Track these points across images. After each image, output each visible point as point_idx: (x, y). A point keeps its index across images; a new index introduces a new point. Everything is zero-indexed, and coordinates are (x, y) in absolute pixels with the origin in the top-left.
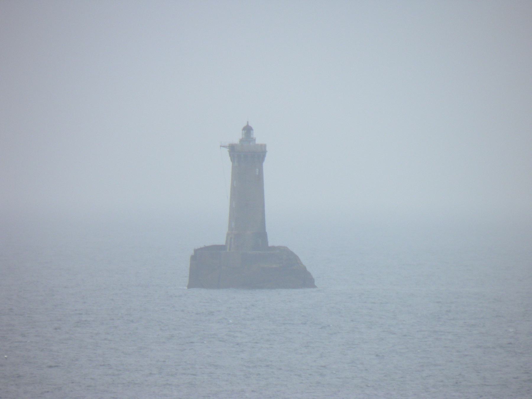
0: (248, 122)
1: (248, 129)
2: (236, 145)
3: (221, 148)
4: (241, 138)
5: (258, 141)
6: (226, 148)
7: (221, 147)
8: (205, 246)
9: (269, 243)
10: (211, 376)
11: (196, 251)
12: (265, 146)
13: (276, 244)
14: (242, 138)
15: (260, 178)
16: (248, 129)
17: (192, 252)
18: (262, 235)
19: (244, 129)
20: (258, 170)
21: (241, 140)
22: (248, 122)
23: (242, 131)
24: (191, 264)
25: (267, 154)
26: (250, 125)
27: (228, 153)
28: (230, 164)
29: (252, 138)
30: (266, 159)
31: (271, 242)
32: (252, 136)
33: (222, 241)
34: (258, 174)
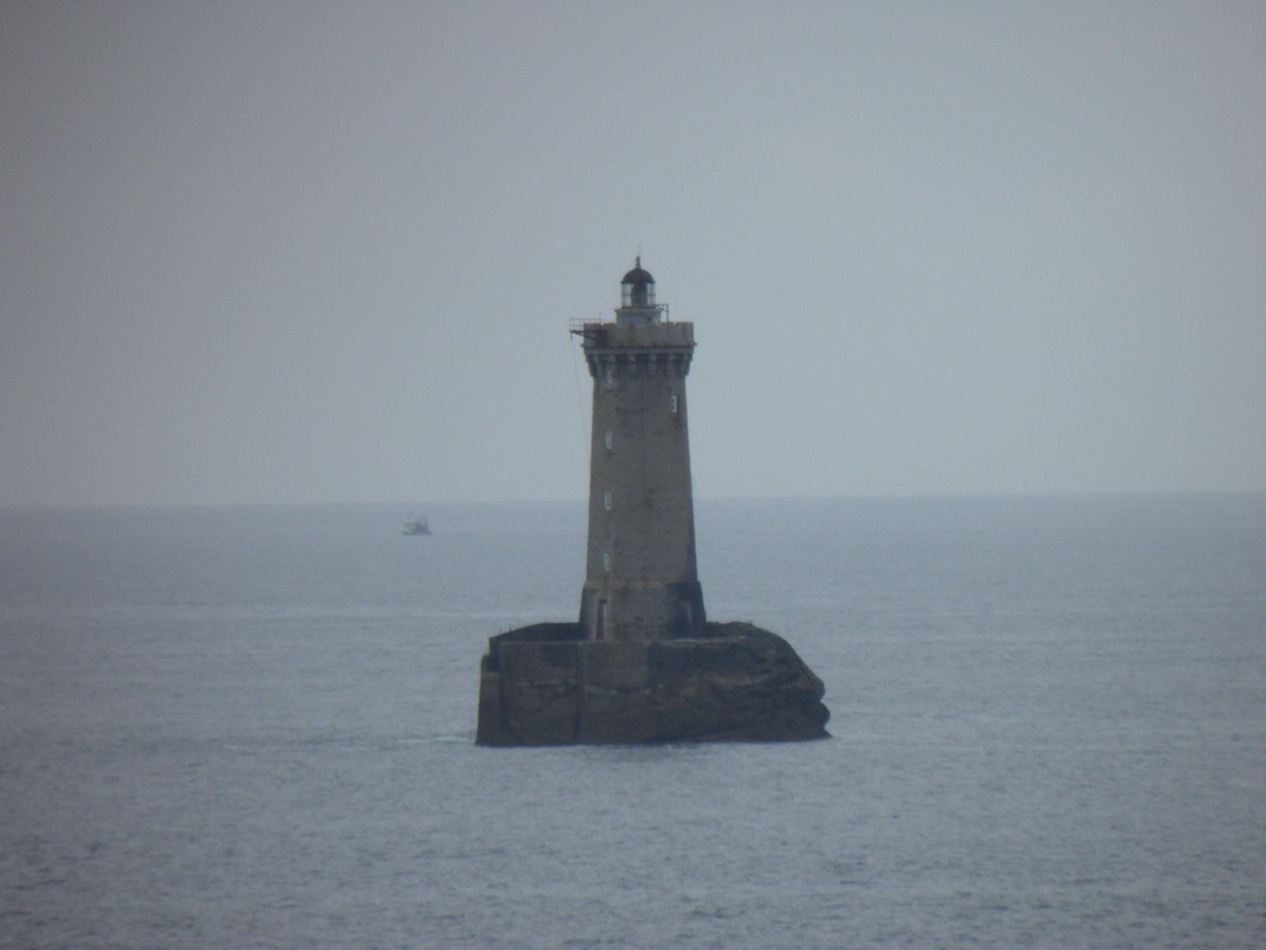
0: (638, 259)
1: (638, 281)
2: (610, 326)
3: (572, 339)
4: (619, 306)
5: (674, 315)
6: (581, 335)
7: (574, 335)
10: (844, 883)
11: (495, 642)
12: (686, 329)
14: (624, 307)
15: (678, 423)
16: (638, 281)
17: (485, 649)
18: (689, 591)
19: (629, 278)
20: (674, 398)
21: (622, 313)
22: (638, 259)
24: (484, 683)
26: (645, 266)
27: (581, 350)
28: (587, 383)
31: (717, 610)
32: (649, 302)
33: (569, 613)
34: (675, 411)
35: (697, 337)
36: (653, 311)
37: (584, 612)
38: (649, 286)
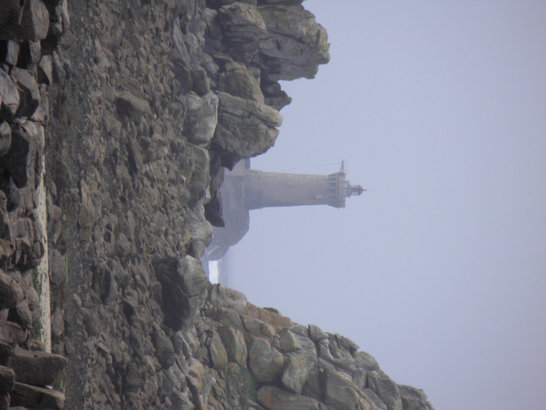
1: (359, 190)
16: (359, 190)
26: (364, 193)
31: (253, 213)
35: (341, 209)
36: (349, 195)
37: (302, 7)
38: (357, 193)
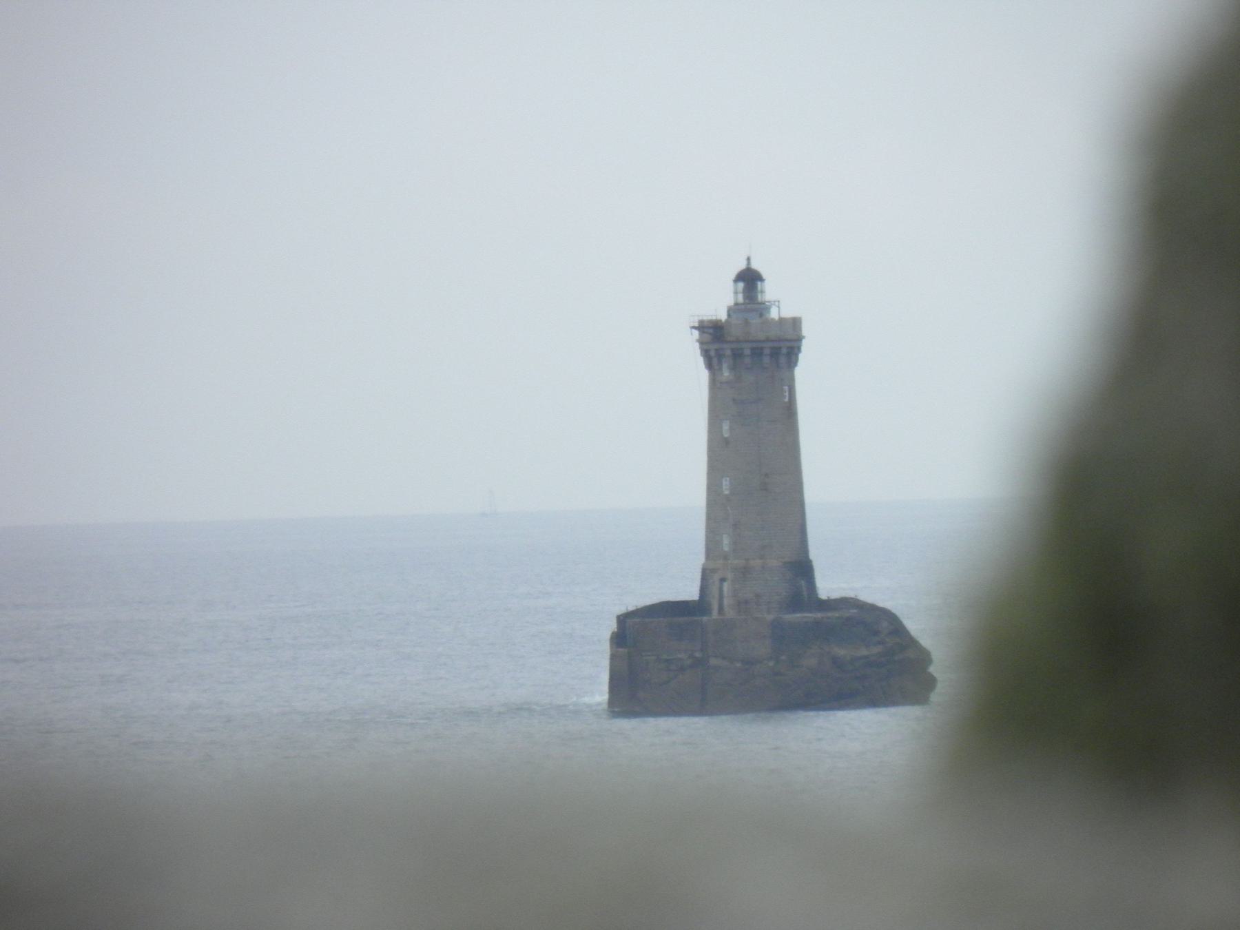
0: (749, 259)
1: (749, 279)
4: (731, 302)
5: (787, 312)
8: (828, 597)
9: (695, 599)
11: (623, 619)
12: (796, 323)
13: (835, 595)
15: (789, 412)
16: (749, 279)
17: (611, 626)
18: (802, 569)
22: (749, 259)
23: (732, 283)
24: (613, 657)
25: (805, 345)
29: (763, 303)
30: (802, 357)
33: (689, 590)
